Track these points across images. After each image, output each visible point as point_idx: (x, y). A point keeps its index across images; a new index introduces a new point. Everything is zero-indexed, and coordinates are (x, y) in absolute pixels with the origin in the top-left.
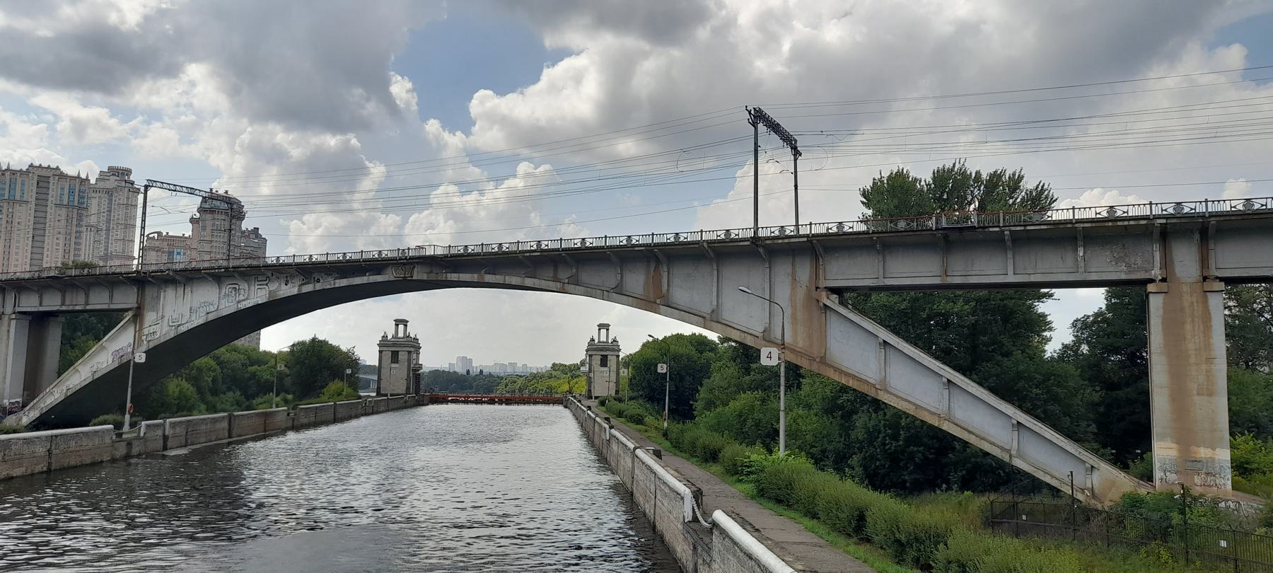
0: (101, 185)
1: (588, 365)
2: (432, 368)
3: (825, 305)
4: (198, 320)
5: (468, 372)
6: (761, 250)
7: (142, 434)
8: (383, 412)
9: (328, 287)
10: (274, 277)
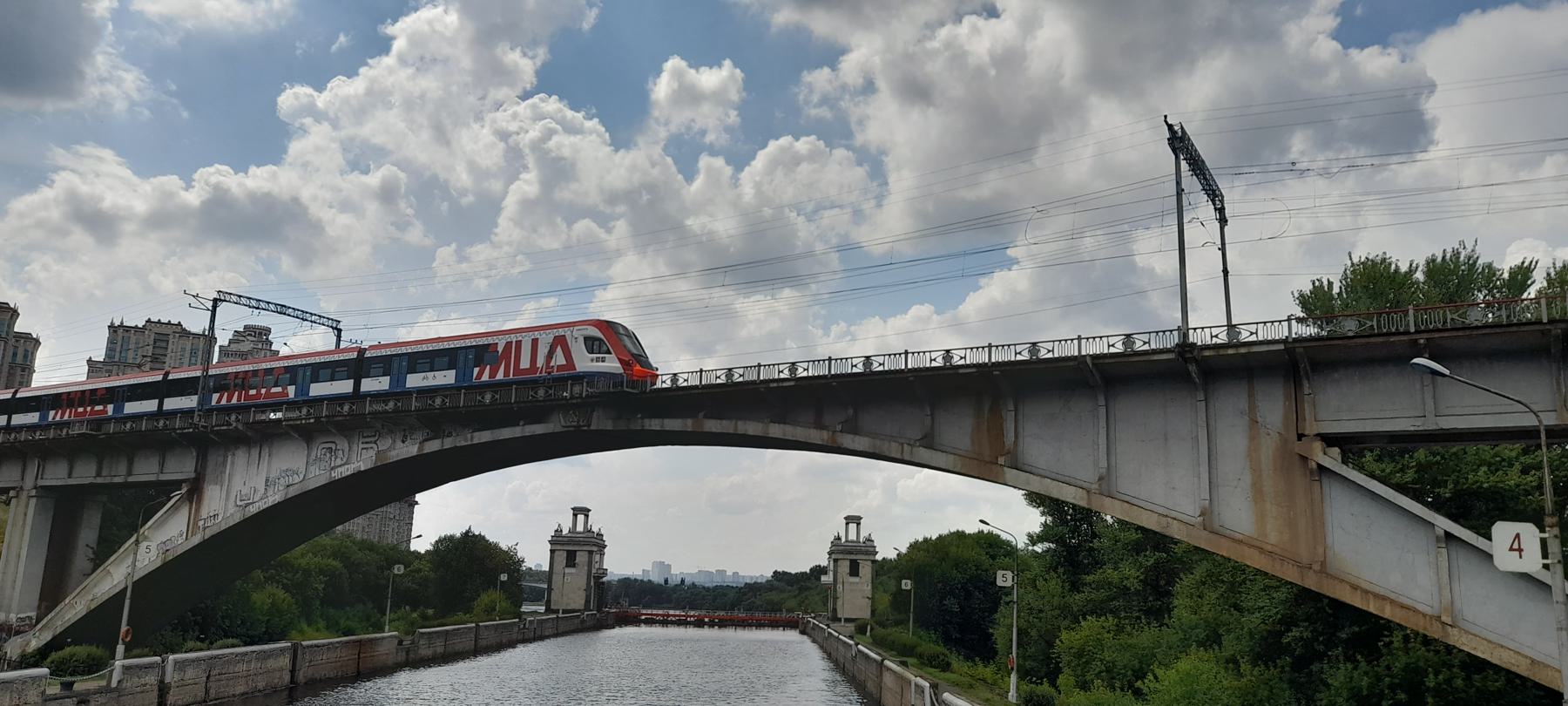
0: (234, 347)
1: (831, 573)
2: (621, 575)
3: (1321, 468)
4: (275, 497)
5: (666, 581)
6: (1192, 368)
7: (114, 684)
8: (548, 637)
9: (463, 443)
10: (386, 430)
